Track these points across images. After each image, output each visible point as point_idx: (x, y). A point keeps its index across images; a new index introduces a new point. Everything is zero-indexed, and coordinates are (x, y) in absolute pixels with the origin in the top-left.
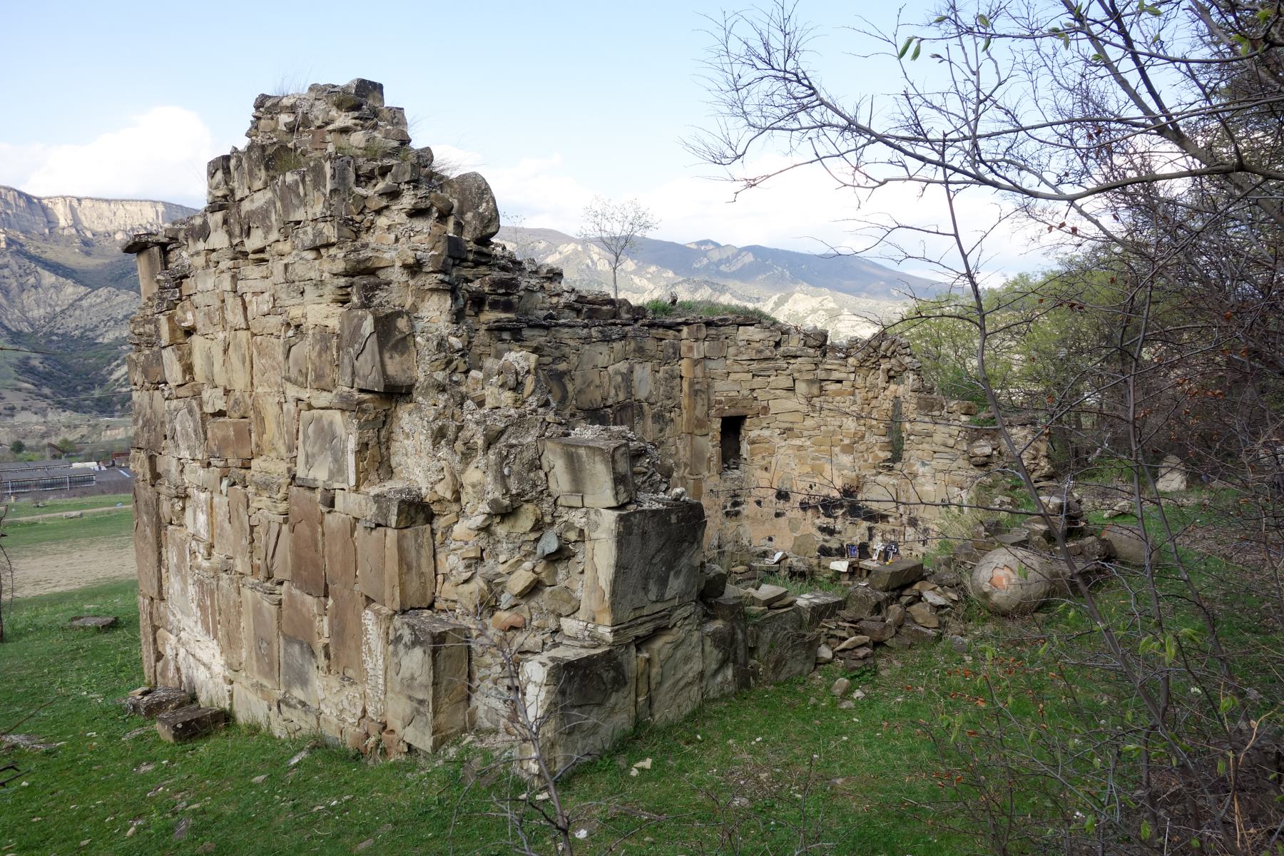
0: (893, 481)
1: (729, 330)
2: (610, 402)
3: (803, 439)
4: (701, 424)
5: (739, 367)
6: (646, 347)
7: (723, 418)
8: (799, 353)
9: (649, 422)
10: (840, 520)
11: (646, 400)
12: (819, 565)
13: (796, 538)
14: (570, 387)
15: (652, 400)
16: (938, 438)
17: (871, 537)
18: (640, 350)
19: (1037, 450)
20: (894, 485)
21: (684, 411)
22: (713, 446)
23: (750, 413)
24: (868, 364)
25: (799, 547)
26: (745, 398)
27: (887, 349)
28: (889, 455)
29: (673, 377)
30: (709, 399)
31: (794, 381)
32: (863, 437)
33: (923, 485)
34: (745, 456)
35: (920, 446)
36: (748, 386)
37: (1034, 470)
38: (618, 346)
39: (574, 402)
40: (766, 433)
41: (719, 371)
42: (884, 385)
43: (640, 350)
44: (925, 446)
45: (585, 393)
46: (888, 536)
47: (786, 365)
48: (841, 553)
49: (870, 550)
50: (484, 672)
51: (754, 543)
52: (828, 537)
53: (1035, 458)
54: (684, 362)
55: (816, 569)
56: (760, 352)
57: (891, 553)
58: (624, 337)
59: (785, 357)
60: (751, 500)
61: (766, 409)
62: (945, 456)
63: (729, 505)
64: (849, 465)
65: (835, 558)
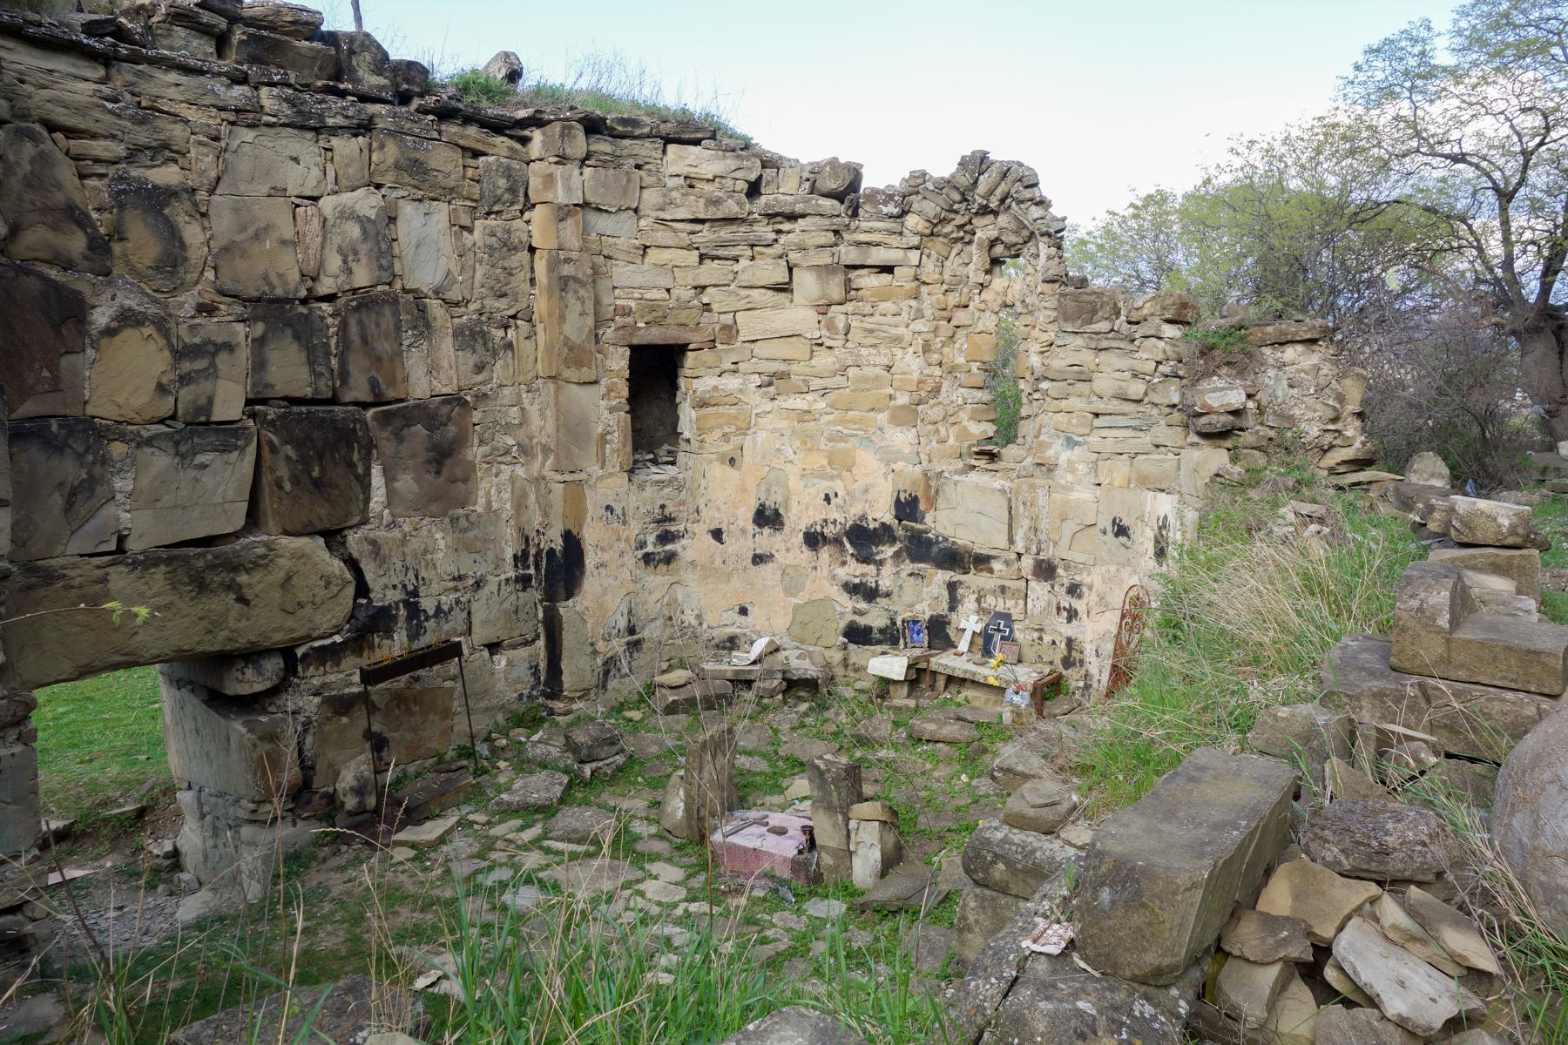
0: (998, 482)
1: (647, 150)
2: (326, 286)
3: (810, 397)
4: (575, 356)
5: (669, 234)
6: (433, 164)
8: (799, 208)
9: (447, 346)
10: (888, 569)
11: (437, 292)
12: (845, 663)
13: (796, 608)
14: (193, 234)
15: (455, 294)
16: (1103, 383)
17: (953, 604)
18: (415, 168)
19: (1341, 398)
20: (1003, 491)
21: (540, 328)
22: (611, 410)
23: (695, 339)
24: (948, 229)
25: (802, 622)
26: (684, 305)
27: (991, 192)
28: (990, 429)
29: (510, 247)
30: (597, 302)
31: (790, 270)
32: (936, 391)
33: (1068, 488)
34: (686, 435)
35: (1063, 404)
36: (690, 278)
37: (1331, 447)
38: (346, 147)
39: (210, 275)
40: (731, 383)
41: (623, 243)
42: (981, 278)
43: (415, 168)
44: (1075, 403)
45: (244, 254)
46: (990, 601)
47: (773, 236)
48: (891, 637)
49: (951, 632)
50: (382, 499)
51: (709, 619)
52: (863, 605)
53: (1334, 420)
54: (537, 215)
55: (839, 671)
56: (716, 202)
57: (997, 637)
58: (365, 127)
59: (770, 216)
60: (702, 529)
61: (730, 331)
62: (1120, 421)
63: (651, 539)
64: (907, 450)
65: (879, 648)
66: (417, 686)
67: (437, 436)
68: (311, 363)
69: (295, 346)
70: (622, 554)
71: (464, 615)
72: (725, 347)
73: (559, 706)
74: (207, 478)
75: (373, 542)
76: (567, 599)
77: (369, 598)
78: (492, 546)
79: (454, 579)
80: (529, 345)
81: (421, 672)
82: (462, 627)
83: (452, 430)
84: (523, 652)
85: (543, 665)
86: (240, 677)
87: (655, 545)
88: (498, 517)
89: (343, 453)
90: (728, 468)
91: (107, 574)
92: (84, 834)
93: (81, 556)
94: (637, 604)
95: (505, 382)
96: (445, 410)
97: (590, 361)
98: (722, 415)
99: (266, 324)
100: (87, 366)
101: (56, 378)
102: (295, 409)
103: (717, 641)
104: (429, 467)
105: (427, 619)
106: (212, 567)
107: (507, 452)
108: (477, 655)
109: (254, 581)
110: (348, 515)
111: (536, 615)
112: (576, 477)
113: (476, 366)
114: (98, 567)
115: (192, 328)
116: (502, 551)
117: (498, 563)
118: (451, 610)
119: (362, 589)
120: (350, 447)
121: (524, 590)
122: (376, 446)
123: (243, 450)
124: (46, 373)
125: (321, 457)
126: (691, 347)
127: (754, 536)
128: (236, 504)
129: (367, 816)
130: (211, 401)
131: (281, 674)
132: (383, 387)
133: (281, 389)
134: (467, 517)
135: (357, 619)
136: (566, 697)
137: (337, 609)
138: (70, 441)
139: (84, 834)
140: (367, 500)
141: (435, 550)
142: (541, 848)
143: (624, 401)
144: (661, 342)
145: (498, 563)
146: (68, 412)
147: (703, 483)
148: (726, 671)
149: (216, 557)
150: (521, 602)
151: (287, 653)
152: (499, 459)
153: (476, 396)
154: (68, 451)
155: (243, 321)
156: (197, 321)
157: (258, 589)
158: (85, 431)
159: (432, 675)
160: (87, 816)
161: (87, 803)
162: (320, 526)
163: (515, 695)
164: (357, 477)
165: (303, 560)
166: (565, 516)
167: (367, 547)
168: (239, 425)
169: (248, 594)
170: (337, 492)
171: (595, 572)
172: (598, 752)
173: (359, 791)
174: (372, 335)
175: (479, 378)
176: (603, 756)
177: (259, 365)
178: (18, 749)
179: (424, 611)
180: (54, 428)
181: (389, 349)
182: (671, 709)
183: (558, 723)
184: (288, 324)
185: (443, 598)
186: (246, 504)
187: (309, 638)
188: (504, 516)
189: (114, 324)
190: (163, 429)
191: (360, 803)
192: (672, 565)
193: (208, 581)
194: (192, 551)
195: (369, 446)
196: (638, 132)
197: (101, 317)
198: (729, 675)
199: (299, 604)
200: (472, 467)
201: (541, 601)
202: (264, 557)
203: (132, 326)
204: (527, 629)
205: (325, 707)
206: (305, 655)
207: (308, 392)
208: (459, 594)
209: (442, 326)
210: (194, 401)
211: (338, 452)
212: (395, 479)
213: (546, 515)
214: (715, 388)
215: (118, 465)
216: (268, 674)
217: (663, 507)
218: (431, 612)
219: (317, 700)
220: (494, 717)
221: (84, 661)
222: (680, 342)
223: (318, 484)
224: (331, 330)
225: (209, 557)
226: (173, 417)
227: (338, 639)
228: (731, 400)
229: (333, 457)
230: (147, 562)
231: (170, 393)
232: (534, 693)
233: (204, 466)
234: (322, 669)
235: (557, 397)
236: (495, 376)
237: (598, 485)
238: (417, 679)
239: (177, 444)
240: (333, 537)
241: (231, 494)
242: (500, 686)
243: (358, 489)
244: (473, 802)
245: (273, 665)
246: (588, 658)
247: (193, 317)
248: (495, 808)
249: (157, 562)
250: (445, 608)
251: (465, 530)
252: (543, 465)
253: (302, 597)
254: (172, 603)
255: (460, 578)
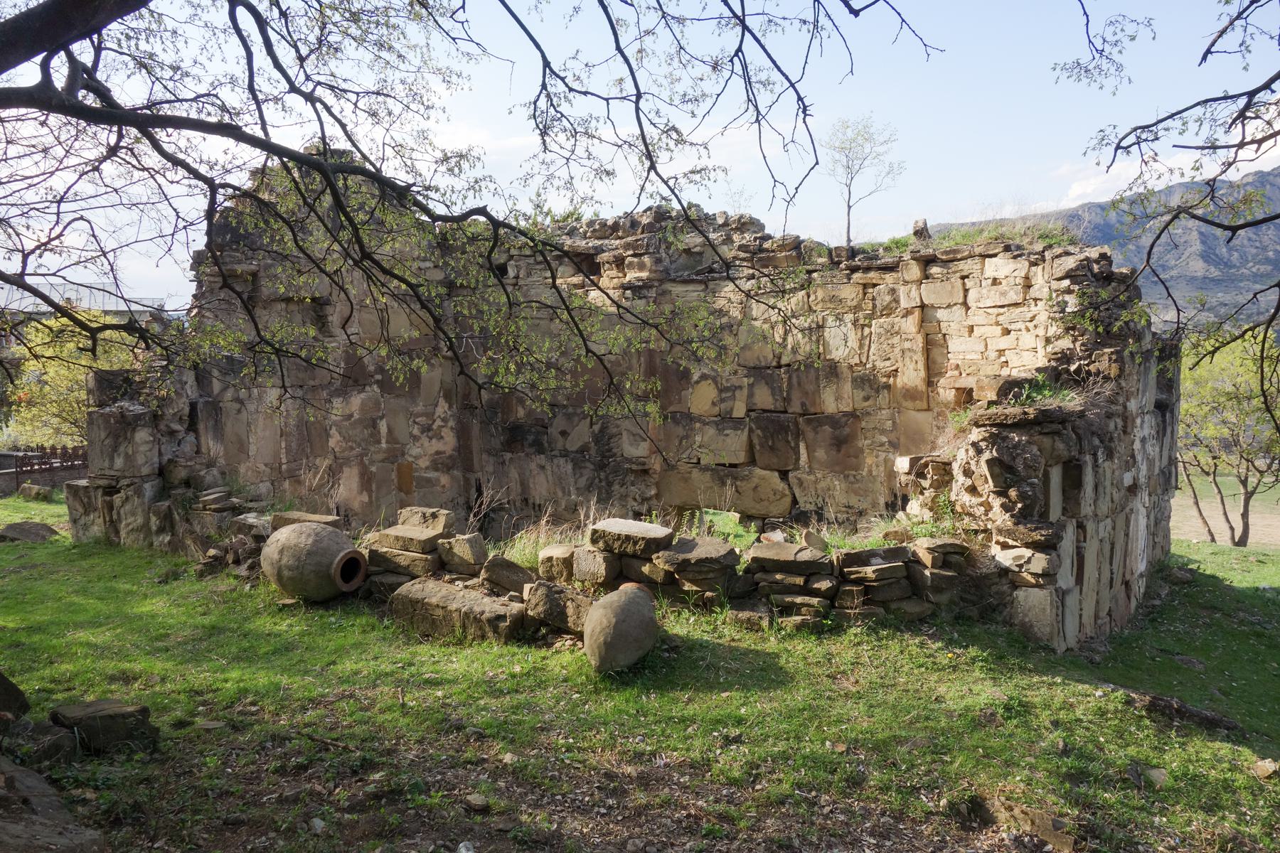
9: (848, 387)
45: (750, 349)
68: (773, 394)
69: (766, 387)
74: (728, 440)
75: (799, 479)
83: (847, 430)
88: (875, 480)
96: (844, 419)
101: (680, 400)
110: (787, 465)
116: (877, 499)
120: (787, 433)
123: (743, 430)
125: (772, 436)
130: (732, 409)
134: (854, 476)
140: (798, 459)
167: (796, 481)
175: (866, 404)
177: (751, 395)
184: (763, 378)
196: (959, 256)
197: (695, 378)
207: (772, 407)
223: (772, 448)
230: (706, 469)
233: (727, 435)
240: (784, 475)
241: (738, 448)
251: (852, 483)
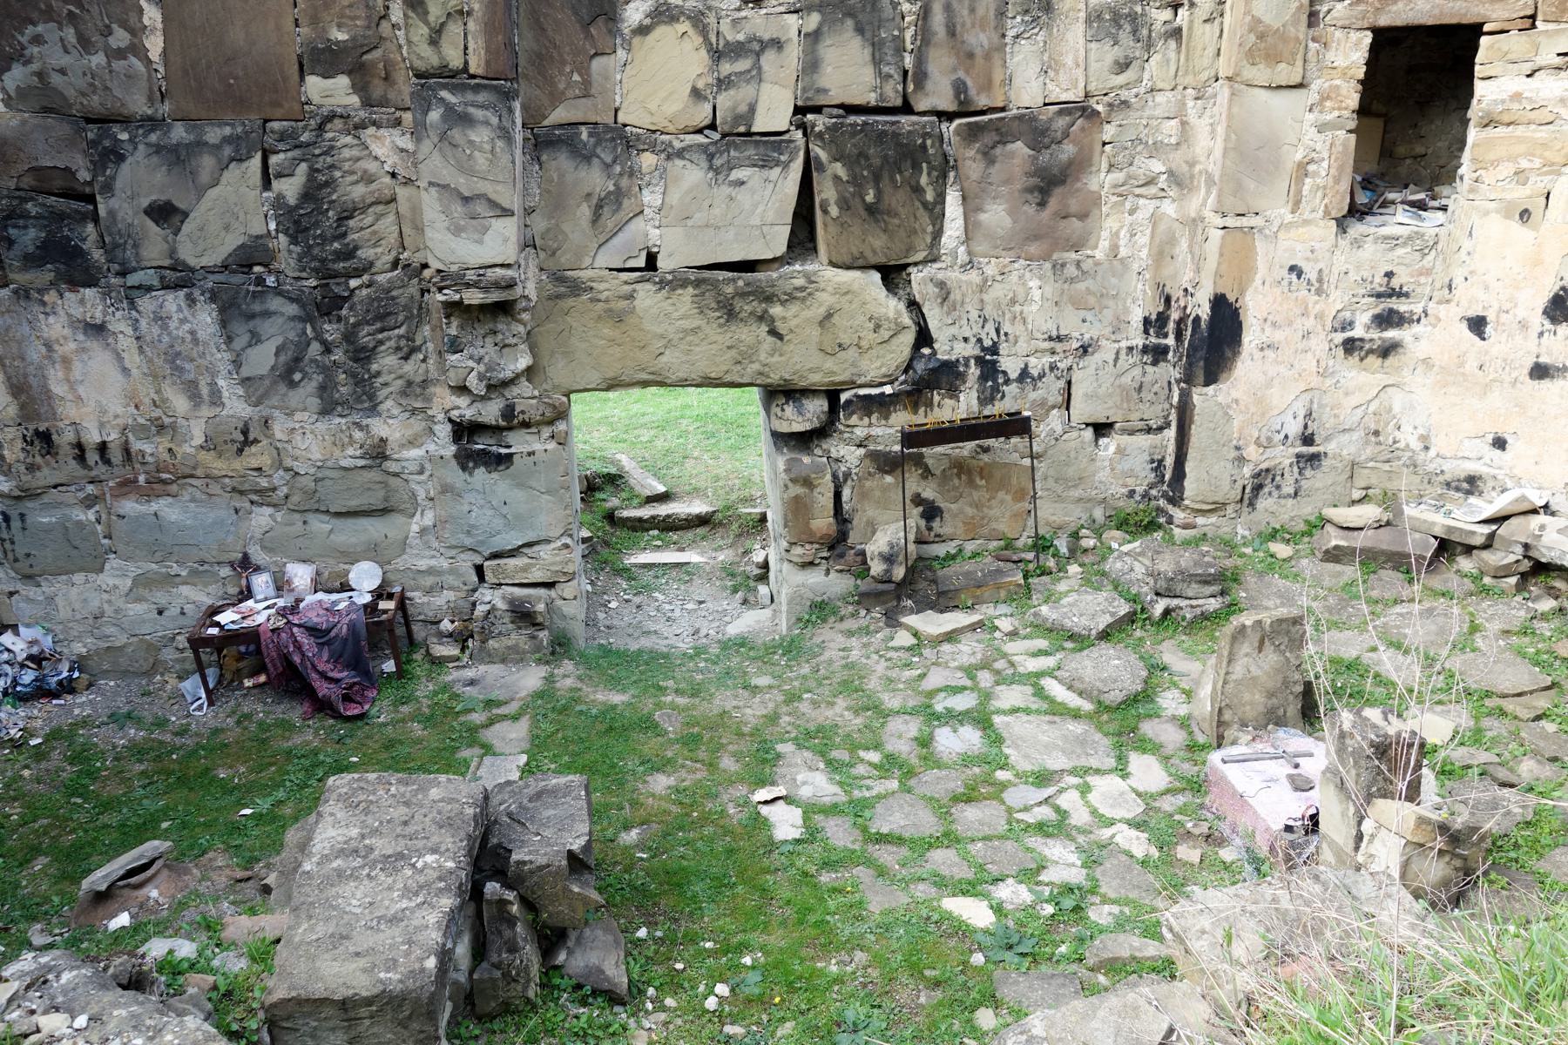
7: (1378, 32)
22: (1322, 128)
50: (957, 234)
51: (1439, 444)
63: (1364, 317)
66: (985, 458)
67: (1044, 157)
68: (877, 62)
70: (1307, 335)
71: (1062, 384)
72: (1551, 26)
73: (1179, 515)
74: (742, 195)
75: (941, 285)
76: (1207, 384)
77: (932, 348)
78: (1111, 303)
79: (1051, 339)
80: (1211, 31)
81: (991, 442)
82: (1056, 398)
83: (1068, 150)
84: (1144, 441)
85: (1169, 461)
86: (779, 414)
87: (1368, 328)
89: (907, 174)
90: (1515, 226)
91: (634, 291)
92: (721, 524)
93: (611, 270)
94: (1321, 406)
95: (1160, 85)
96: (1062, 122)
97: (1294, 54)
98: (1521, 140)
99: (823, 14)
100: (618, 69)
101: (587, 83)
102: (852, 119)
103: (1448, 477)
104: (1029, 197)
105: (1007, 382)
106: (742, 295)
107: (1150, 182)
108: (1075, 434)
109: (789, 314)
110: (910, 249)
111: (1169, 397)
112: (1244, 222)
113: (1117, 63)
114: (626, 283)
115: (735, 22)
116: (1127, 311)
117: (1118, 327)
118: (1041, 376)
119: (924, 337)
120: (916, 167)
121: (1155, 363)
122: (955, 168)
123: (786, 165)
124: (576, 77)
125: (877, 178)
126: (1486, 28)
127: (1541, 334)
128: (776, 228)
129: (891, 587)
130: (752, 109)
131: (823, 417)
132: (972, 92)
133: (837, 95)
134: (1078, 264)
135: (915, 371)
136: (1187, 507)
137: (889, 356)
138: (598, 151)
139: (721, 524)
140: (938, 234)
141: (1027, 300)
142: (1035, 685)
143: (1346, 114)
144: (1430, 22)
145: (1118, 327)
146: (599, 120)
147: (1467, 245)
148: (1434, 523)
149: (748, 284)
150: (1148, 378)
151: (832, 395)
152: (1138, 191)
153: (1110, 105)
154: (595, 161)
155: (796, 12)
156: (743, 14)
157: (793, 323)
158: (613, 139)
159: (1008, 449)
160: (728, 508)
161: (734, 497)
162: (874, 260)
163: (1125, 491)
164: (925, 205)
165: (849, 297)
166: (1218, 275)
167: (932, 290)
168: (786, 137)
169: (781, 327)
170: (896, 221)
171: (1257, 355)
172: (1179, 587)
173: (889, 559)
174: (963, 25)
176: (1190, 594)
177: (811, 65)
178: (551, 446)
179: (1004, 373)
180: (584, 136)
181: (986, 43)
182: (1335, 556)
183: (1172, 537)
185: (1033, 361)
186: (789, 228)
187: (853, 384)
188: (1135, 267)
189: (648, 21)
190: (700, 139)
191: (887, 571)
192: (1391, 360)
193: (737, 310)
194: (722, 275)
195: (944, 168)
198: (1439, 532)
199: (840, 345)
200: (1096, 200)
201: (1178, 381)
202: (802, 289)
203: (666, 23)
204: (1154, 414)
205: (867, 462)
206: (848, 402)
207: (872, 99)
208: (1056, 358)
209: (1072, 9)
210: (734, 108)
211: (900, 172)
212: (979, 209)
213: (1198, 271)
214: (1517, 97)
215: (647, 178)
216: (809, 416)
217: (1389, 275)
218: (1013, 375)
219: (862, 451)
220: (1090, 510)
221: (610, 374)
222: (1468, 19)
223: (872, 210)
224: (907, 19)
225: (741, 283)
226: (712, 126)
227: (888, 390)
228: (1543, 115)
229: (893, 180)
230: (676, 282)
231: (706, 98)
232: (1154, 492)
234: (866, 420)
235: (1229, 108)
236: (1146, 76)
237: (1281, 235)
238: (986, 450)
239: (711, 157)
240: (892, 275)
242: (1103, 475)
243: (924, 218)
244: (1014, 605)
245: (816, 408)
246: (1229, 465)
247: (739, 9)
248: (1032, 618)
249: (684, 283)
250: (1035, 373)
251: (1072, 280)
252: (1204, 204)
253: (845, 340)
254: (699, 328)
255: (1059, 339)
